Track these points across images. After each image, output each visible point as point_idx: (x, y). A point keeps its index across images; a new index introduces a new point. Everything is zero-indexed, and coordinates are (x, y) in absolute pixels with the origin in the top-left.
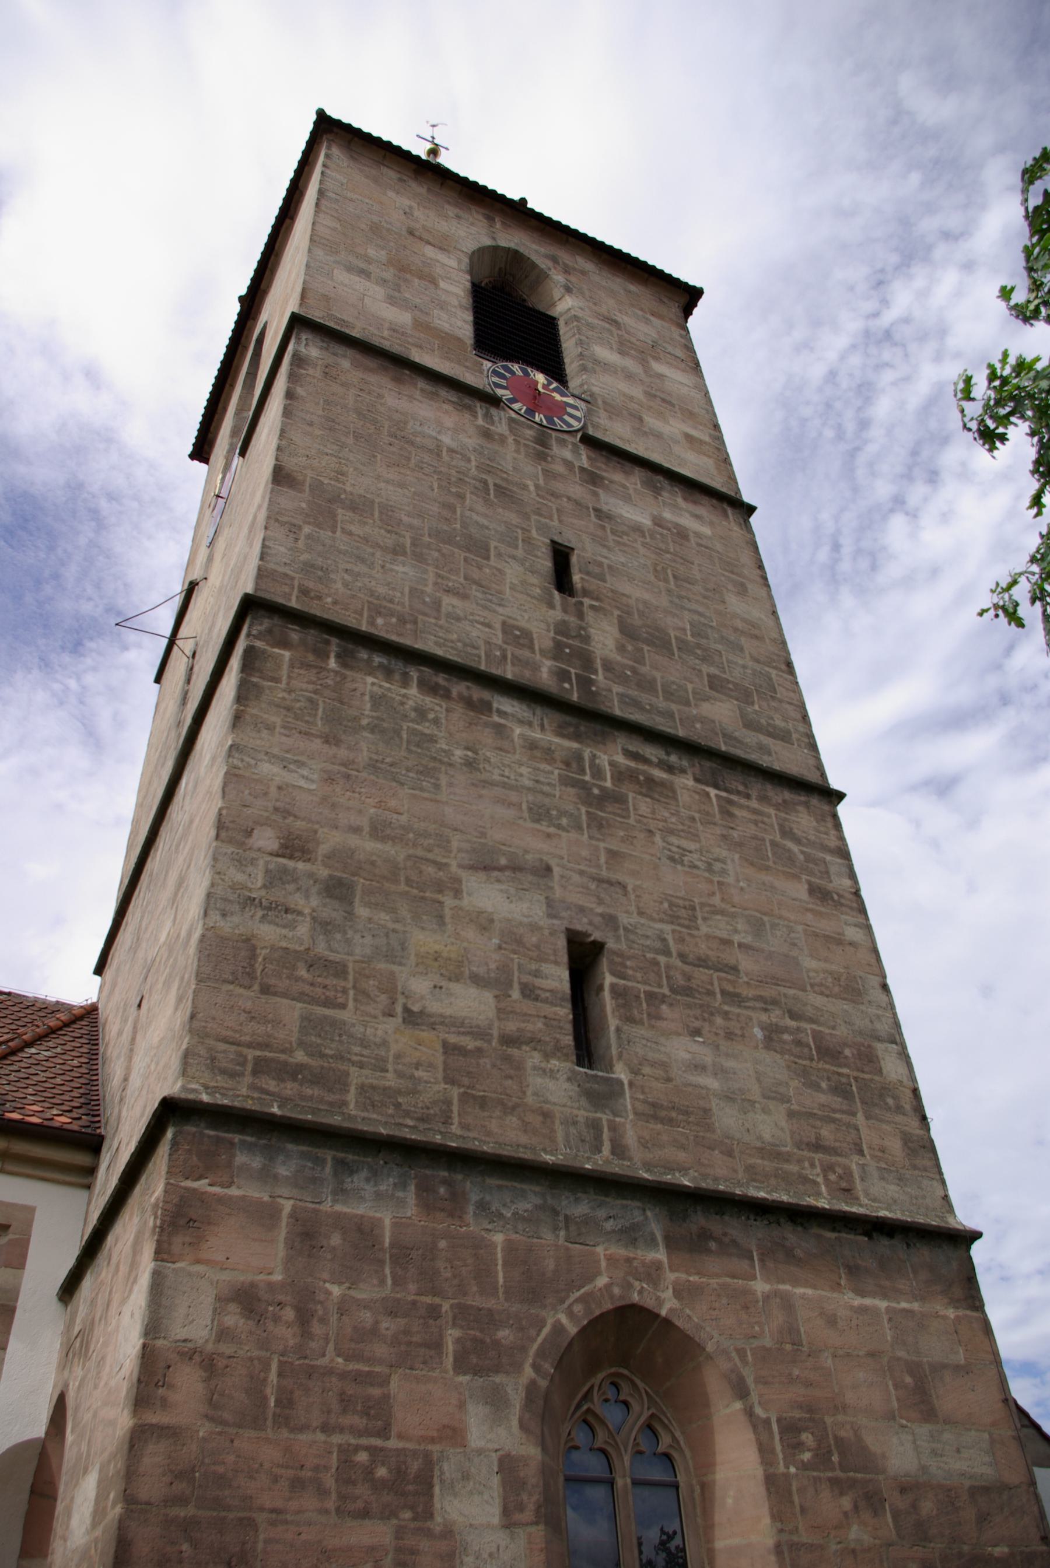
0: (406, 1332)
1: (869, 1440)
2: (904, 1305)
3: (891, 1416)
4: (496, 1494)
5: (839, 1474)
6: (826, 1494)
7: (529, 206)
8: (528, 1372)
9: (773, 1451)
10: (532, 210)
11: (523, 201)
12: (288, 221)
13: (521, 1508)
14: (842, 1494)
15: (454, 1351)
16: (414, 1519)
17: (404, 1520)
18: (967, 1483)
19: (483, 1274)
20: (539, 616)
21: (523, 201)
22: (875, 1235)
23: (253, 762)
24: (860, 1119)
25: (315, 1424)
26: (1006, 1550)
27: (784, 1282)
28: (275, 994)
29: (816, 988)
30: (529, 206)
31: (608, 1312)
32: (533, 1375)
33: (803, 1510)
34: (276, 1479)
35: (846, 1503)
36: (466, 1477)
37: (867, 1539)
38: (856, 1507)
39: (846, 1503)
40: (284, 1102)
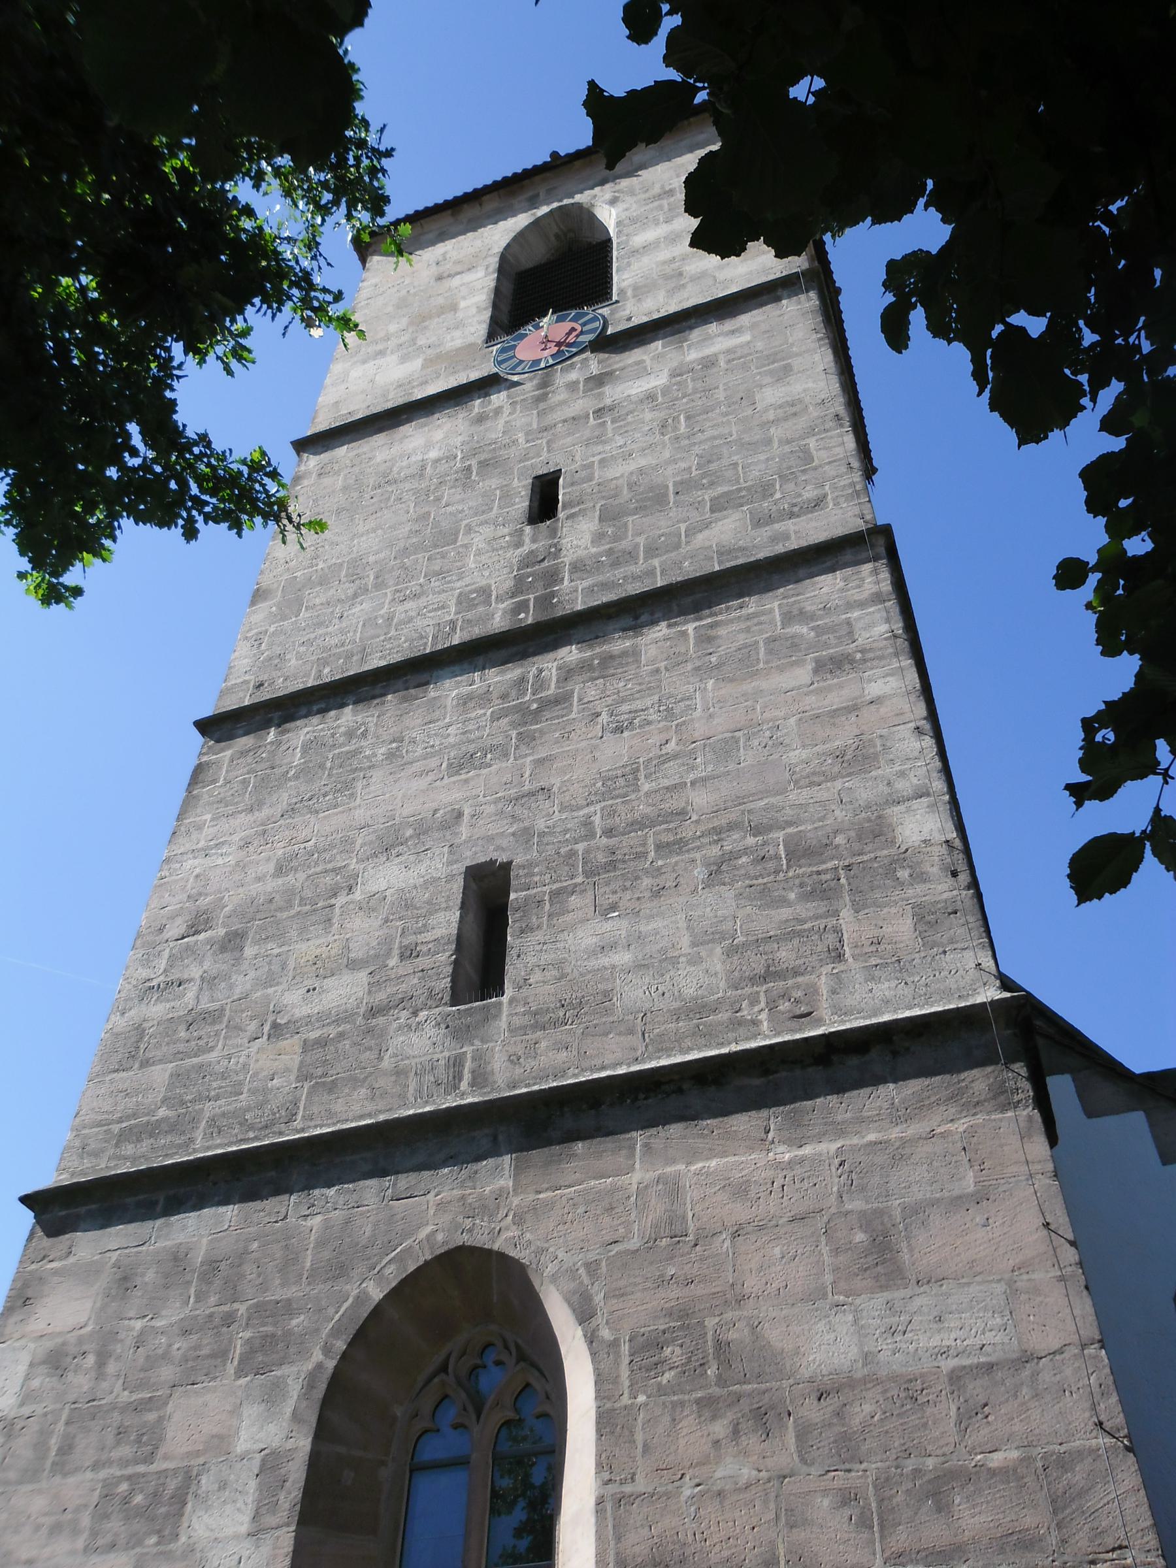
0: (197, 1347)
1: (774, 1335)
2: (872, 1137)
3: (815, 1296)
4: (250, 1500)
5: (716, 1391)
6: (688, 1422)
7: (562, 154)
8: (317, 1356)
9: (616, 1380)
10: (568, 155)
11: (555, 155)
12: (628, 621)
13: (274, 1507)
14: (714, 1418)
15: (241, 1354)
16: (158, 1543)
17: (149, 1546)
18: (948, 1364)
19: (291, 1260)
20: (886, 790)
21: (555, 155)
22: (835, 1058)
23: (178, 865)
24: (846, 914)
25: (87, 1464)
26: (1015, 1454)
27: (674, 1162)
28: (153, 1064)
29: (802, 783)
30: (562, 154)
31: (427, 1263)
32: (321, 1357)
33: (646, 1448)
34: (38, 1528)
35: (720, 1428)
36: (223, 1486)
37: (747, 1473)
38: (736, 1432)
39: (720, 1428)
40: (134, 1159)
